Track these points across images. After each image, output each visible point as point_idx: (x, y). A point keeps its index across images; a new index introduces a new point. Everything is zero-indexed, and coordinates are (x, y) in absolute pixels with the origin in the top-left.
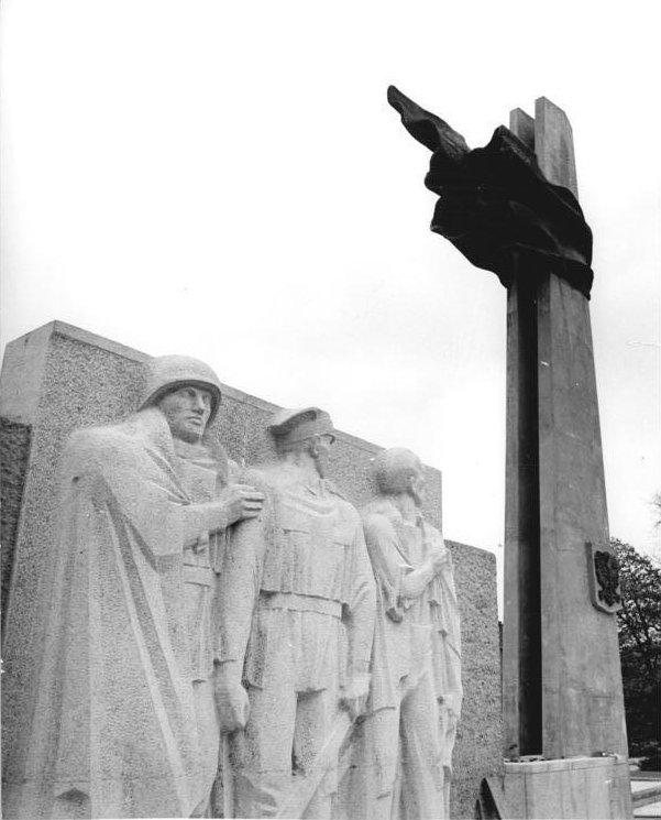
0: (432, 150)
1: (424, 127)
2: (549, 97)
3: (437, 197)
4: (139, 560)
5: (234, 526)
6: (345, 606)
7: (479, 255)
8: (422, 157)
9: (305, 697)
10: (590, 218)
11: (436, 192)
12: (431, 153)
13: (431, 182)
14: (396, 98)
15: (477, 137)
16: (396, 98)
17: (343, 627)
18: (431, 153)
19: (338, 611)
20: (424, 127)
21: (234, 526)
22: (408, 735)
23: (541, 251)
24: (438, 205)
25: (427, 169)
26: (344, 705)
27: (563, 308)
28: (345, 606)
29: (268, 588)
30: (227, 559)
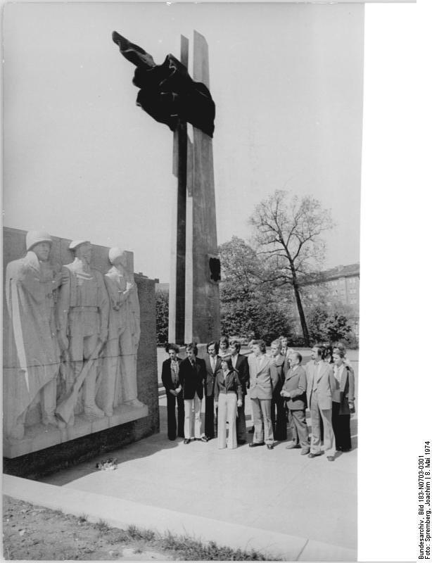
0: (136, 65)
1: (132, 52)
2: (134, 254)
3: (138, 89)
4: (32, 303)
5: (60, 287)
6: (98, 308)
7: (159, 117)
8: (131, 68)
9: (86, 339)
10: (214, 98)
11: (135, 64)
12: (135, 67)
13: (136, 81)
14: (117, 38)
15: (159, 61)
16: (117, 38)
17: (98, 315)
18: (135, 67)
19: (96, 310)
20: (132, 52)
21: (60, 287)
22: (122, 347)
23: (201, 93)
24: (140, 94)
25: (133, 75)
26: (99, 340)
27: (70, 295)
28: (98, 308)
29: (72, 305)
30: (59, 298)
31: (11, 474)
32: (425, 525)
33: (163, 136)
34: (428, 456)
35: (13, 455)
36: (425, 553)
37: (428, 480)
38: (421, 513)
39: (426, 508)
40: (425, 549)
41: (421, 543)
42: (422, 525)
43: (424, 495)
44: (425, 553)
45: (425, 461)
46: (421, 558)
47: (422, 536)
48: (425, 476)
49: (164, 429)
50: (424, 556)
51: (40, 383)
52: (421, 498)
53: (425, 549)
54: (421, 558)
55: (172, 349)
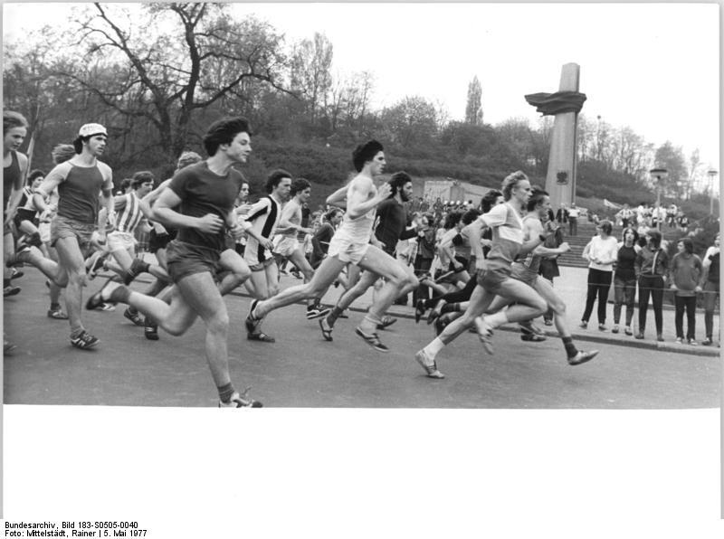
31: (562, 75)
32: (49, 530)
33: (153, 255)
34: (128, 533)
35: (571, 115)
36: (13, 530)
37: (97, 534)
38: (64, 525)
39: (68, 531)
40: (17, 530)
41: (25, 526)
42: (49, 526)
43: (84, 529)
44: (13, 530)
45: (122, 530)
46: (7, 525)
47: (35, 526)
48: (103, 529)
49: (582, 190)
50: (9, 529)
51: (557, 350)
52: (84, 525)
53: (17, 530)
54: (7, 525)
55: (532, 168)
